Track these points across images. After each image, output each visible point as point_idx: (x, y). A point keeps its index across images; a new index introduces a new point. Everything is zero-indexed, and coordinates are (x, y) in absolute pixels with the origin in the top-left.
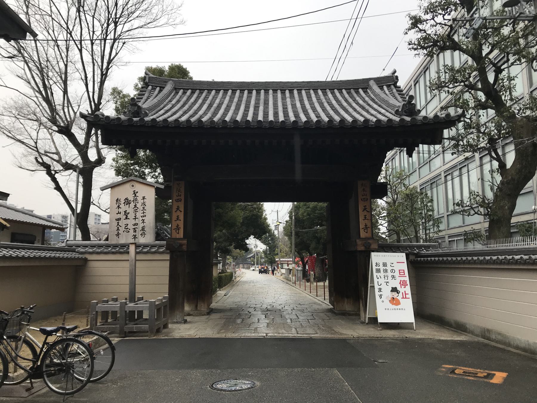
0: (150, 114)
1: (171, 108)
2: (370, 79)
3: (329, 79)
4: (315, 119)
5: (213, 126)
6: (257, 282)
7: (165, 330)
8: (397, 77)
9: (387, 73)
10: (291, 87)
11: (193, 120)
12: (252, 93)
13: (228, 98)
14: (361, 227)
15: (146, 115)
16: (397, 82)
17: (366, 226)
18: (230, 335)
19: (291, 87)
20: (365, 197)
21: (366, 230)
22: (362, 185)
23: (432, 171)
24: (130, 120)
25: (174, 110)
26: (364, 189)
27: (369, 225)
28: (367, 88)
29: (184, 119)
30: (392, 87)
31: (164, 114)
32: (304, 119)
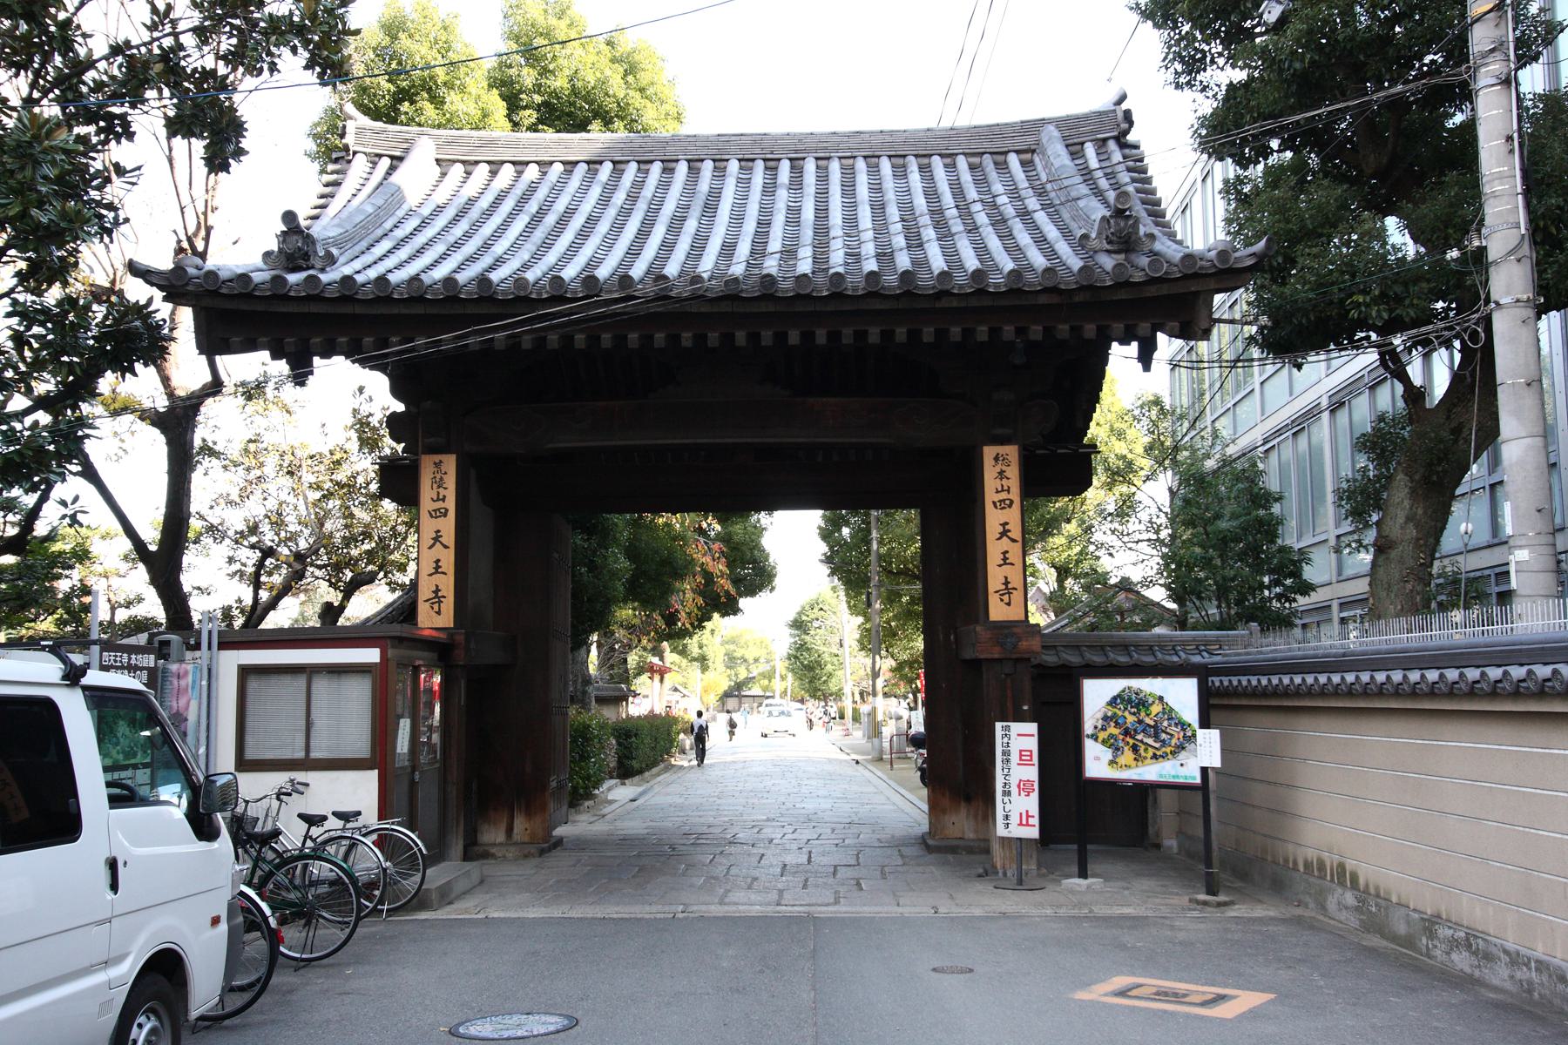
0: (342, 260)
1: (468, 235)
2: (1044, 122)
3: (946, 124)
4: (1038, 260)
5: (522, 294)
6: (516, 859)
7: (1496, 610)
8: (1128, 116)
9: (1100, 100)
10: (796, 151)
11: (462, 278)
12: (672, 171)
13: (596, 191)
14: (991, 589)
15: (331, 260)
16: (1127, 132)
17: (1006, 583)
18: (1150, 772)
19: (796, 151)
20: (1004, 495)
21: (1006, 598)
22: (996, 459)
23: (1296, 392)
24: (278, 280)
25: (421, 239)
26: (1001, 473)
27: (1016, 581)
28: (1033, 151)
29: (439, 273)
30: (1112, 145)
31: (411, 258)
32: (938, 263)
